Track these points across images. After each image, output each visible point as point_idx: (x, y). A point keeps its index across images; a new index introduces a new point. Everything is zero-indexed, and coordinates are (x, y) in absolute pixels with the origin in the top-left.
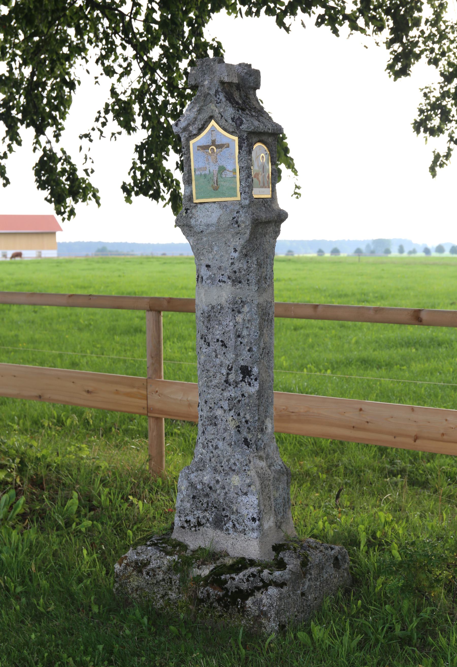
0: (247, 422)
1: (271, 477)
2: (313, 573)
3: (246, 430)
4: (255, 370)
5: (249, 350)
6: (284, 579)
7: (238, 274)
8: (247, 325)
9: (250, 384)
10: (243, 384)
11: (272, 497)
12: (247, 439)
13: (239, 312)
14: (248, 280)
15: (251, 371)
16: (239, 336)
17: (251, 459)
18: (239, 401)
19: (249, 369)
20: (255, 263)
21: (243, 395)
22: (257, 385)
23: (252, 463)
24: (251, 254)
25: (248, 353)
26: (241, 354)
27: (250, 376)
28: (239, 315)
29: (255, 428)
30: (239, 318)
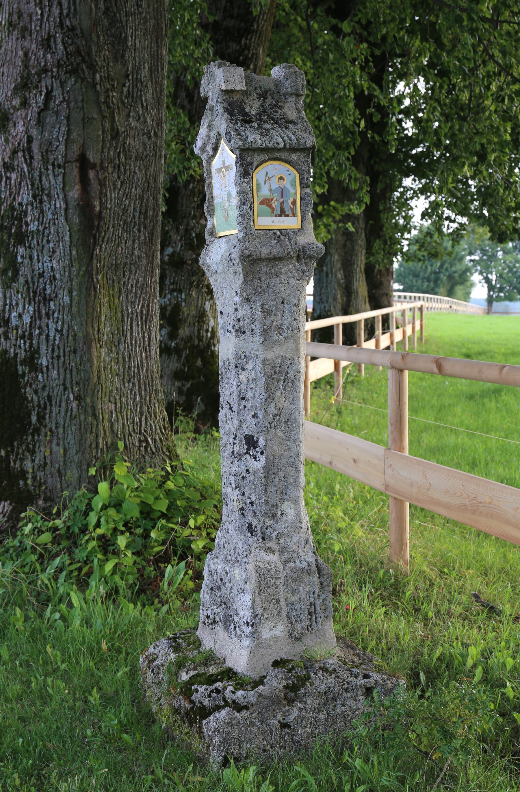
0: (252, 504)
1: (282, 576)
2: (309, 702)
3: (251, 513)
4: (262, 442)
5: (254, 416)
6: (248, 702)
7: (242, 323)
8: (252, 386)
9: (255, 458)
10: (248, 456)
11: (282, 600)
12: (251, 525)
13: (243, 369)
14: (252, 331)
15: (257, 442)
16: (243, 398)
17: (253, 550)
18: (244, 478)
19: (255, 439)
20: (260, 309)
21: (247, 471)
22: (263, 458)
23: (252, 555)
24: (254, 298)
25: (253, 420)
26: (244, 421)
27: (255, 448)
28: (244, 373)
29: (261, 512)
30: (243, 377)
